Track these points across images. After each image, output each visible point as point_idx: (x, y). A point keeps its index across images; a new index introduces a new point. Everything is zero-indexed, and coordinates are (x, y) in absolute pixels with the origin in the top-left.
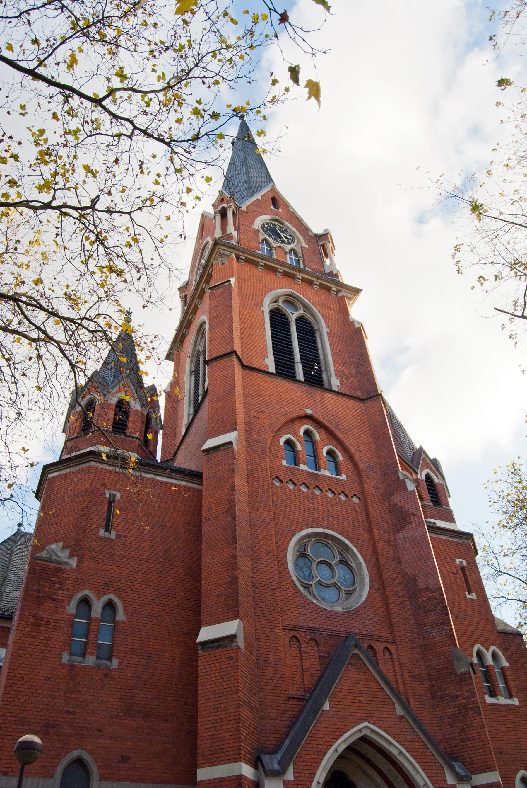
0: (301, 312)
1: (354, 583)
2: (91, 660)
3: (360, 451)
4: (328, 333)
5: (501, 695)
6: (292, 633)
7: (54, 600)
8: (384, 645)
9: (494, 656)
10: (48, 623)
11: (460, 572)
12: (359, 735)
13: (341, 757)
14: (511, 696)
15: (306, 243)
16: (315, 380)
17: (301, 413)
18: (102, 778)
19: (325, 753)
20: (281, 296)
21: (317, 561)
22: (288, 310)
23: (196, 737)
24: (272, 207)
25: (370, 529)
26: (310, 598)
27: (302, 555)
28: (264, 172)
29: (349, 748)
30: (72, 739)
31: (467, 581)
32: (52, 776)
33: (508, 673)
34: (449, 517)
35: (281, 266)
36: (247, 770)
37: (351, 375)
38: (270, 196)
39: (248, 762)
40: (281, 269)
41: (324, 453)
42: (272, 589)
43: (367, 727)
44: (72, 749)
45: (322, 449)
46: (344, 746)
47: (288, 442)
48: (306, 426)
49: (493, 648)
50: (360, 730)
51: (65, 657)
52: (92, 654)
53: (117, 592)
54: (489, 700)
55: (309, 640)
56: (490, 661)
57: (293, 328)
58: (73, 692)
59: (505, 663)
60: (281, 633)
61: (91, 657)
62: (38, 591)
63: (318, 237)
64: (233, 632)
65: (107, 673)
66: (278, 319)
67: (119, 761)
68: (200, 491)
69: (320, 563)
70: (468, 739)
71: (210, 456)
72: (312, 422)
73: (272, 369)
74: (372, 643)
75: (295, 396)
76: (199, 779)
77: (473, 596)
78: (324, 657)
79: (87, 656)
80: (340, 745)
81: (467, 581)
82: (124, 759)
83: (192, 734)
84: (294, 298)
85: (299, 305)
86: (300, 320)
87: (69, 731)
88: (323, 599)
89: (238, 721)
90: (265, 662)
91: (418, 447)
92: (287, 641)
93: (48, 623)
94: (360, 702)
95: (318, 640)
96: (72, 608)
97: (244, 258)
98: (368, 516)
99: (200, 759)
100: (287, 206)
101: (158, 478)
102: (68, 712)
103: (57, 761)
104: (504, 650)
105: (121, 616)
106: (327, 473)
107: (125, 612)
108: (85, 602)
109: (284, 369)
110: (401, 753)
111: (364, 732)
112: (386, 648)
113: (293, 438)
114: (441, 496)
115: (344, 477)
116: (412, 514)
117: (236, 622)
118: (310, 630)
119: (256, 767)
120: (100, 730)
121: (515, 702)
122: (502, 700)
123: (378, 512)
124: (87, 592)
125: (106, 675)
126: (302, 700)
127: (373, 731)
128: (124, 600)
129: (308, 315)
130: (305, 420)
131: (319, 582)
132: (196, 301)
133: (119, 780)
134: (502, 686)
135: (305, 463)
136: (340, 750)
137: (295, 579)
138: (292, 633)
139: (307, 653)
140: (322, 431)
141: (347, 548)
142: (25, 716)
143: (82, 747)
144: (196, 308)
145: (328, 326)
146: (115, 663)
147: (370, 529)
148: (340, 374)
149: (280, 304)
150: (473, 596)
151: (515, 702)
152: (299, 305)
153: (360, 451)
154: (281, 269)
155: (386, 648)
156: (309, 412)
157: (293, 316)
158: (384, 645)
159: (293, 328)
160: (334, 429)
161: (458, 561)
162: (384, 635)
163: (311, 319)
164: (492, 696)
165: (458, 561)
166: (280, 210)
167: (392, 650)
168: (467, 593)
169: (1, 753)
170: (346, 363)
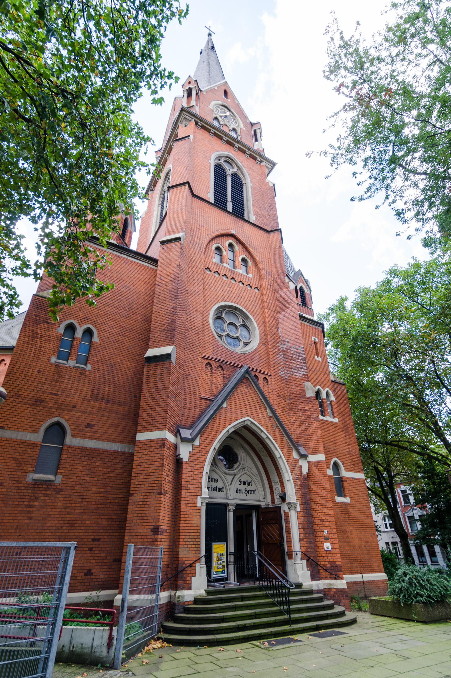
0: (235, 169)
1: (250, 339)
2: (72, 363)
3: (262, 262)
4: (251, 187)
5: (329, 416)
6: (207, 361)
7: (48, 323)
8: (264, 376)
9: (327, 394)
10: (42, 337)
11: (314, 344)
12: (243, 424)
13: (229, 437)
14: (334, 417)
15: (245, 126)
16: (239, 213)
17: (228, 232)
18: (72, 436)
19: (221, 432)
20: (224, 157)
21: (228, 322)
22: (226, 166)
23: (140, 399)
24: (224, 97)
25: (263, 309)
26: (221, 342)
27: (219, 318)
28: (221, 75)
29: (235, 432)
30: (53, 410)
31: (317, 350)
32: (37, 432)
33: (334, 405)
34: (311, 311)
35: (226, 136)
36: (171, 438)
37: (263, 215)
38: (223, 88)
39: (171, 431)
40: (225, 138)
41: (240, 260)
42: (198, 333)
43: (248, 420)
44: (53, 417)
45: (239, 257)
46: (233, 430)
47: (218, 249)
48: (230, 241)
49: (327, 389)
50: (244, 421)
51: (54, 360)
52: (72, 359)
53: (94, 324)
54: (321, 417)
55: (218, 366)
56: (324, 396)
57: (229, 179)
58: (57, 381)
59: (332, 398)
60: (201, 360)
61: (72, 362)
62: (37, 316)
63: (252, 124)
64: (169, 352)
65: (82, 372)
66: (219, 172)
67: (86, 427)
68: (156, 270)
69: (230, 324)
70: (308, 435)
71: (164, 246)
72: (234, 239)
73: (212, 201)
74: (257, 374)
75: (226, 223)
76: (137, 439)
77: (320, 359)
78: (227, 378)
79: (69, 361)
80: (230, 428)
81: (317, 350)
82: (89, 426)
83: (136, 414)
84: (232, 160)
85: (234, 165)
86: (234, 176)
87: (52, 405)
88: (229, 344)
89: (167, 406)
90: (189, 375)
91: (297, 270)
92: (204, 365)
93: (42, 337)
94: (246, 405)
95: (223, 367)
96: (61, 329)
97: (201, 125)
98: (263, 300)
99: (139, 428)
100: (234, 98)
101: (129, 258)
102: (52, 394)
103: (42, 423)
104: (334, 391)
105: (95, 339)
106: (240, 272)
107: (99, 336)
108: (71, 328)
109: (220, 203)
110: (268, 437)
111: (247, 423)
112: (265, 378)
113: (221, 246)
114: (308, 300)
115: (251, 276)
116: (291, 303)
117: (172, 347)
118: (219, 361)
119: (176, 436)
120: (74, 407)
121: (336, 420)
122: (328, 418)
123: (268, 299)
124: (72, 321)
125: (82, 374)
126: (210, 400)
127: (252, 422)
128: (98, 330)
129: (239, 173)
130: (230, 238)
131: (228, 335)
132: (166, 155)
133: (85, 438)
134: (330, 411)
135: (227, 263)
136: (231, 431)
137: (213, 330)
138: (207, 361)
139: (216, 373)
140: (241, 246)
141: (247, 317)
142: (20, 393)
143: (60, 416)
144: (166, 161)
145: (252, 182)
146: (89, 367)
147: (263, 309)
148: (256, 214)
149: (222, 162)
150: (320, 359)
151: (336, 420)
152: (234, 165)
153: (262, 262)
154: (225, 138)
155: (265, 378)
156: (233, 232)
157: (230, 171)
158: (264, 376)
159: (229, 179)
160: (248, 246)
161: (313, 338)
162: (264, 370)
163: (241, 176)
164: (323, 415)
165: (313, 338)
166: (229, 100)
167: (269, 380)
168: (316, 357)
169: (2, 450)
170: (260, 207)
